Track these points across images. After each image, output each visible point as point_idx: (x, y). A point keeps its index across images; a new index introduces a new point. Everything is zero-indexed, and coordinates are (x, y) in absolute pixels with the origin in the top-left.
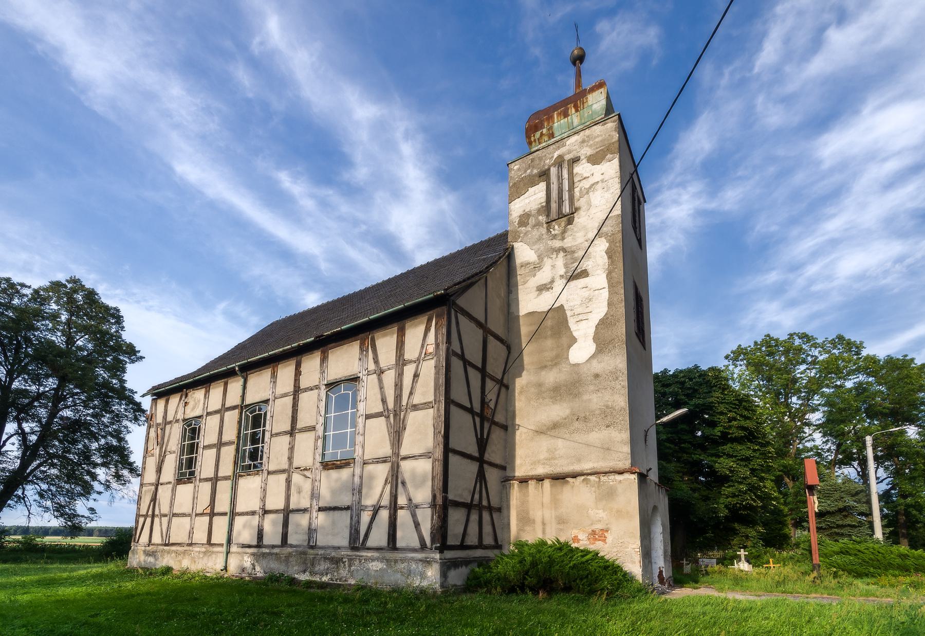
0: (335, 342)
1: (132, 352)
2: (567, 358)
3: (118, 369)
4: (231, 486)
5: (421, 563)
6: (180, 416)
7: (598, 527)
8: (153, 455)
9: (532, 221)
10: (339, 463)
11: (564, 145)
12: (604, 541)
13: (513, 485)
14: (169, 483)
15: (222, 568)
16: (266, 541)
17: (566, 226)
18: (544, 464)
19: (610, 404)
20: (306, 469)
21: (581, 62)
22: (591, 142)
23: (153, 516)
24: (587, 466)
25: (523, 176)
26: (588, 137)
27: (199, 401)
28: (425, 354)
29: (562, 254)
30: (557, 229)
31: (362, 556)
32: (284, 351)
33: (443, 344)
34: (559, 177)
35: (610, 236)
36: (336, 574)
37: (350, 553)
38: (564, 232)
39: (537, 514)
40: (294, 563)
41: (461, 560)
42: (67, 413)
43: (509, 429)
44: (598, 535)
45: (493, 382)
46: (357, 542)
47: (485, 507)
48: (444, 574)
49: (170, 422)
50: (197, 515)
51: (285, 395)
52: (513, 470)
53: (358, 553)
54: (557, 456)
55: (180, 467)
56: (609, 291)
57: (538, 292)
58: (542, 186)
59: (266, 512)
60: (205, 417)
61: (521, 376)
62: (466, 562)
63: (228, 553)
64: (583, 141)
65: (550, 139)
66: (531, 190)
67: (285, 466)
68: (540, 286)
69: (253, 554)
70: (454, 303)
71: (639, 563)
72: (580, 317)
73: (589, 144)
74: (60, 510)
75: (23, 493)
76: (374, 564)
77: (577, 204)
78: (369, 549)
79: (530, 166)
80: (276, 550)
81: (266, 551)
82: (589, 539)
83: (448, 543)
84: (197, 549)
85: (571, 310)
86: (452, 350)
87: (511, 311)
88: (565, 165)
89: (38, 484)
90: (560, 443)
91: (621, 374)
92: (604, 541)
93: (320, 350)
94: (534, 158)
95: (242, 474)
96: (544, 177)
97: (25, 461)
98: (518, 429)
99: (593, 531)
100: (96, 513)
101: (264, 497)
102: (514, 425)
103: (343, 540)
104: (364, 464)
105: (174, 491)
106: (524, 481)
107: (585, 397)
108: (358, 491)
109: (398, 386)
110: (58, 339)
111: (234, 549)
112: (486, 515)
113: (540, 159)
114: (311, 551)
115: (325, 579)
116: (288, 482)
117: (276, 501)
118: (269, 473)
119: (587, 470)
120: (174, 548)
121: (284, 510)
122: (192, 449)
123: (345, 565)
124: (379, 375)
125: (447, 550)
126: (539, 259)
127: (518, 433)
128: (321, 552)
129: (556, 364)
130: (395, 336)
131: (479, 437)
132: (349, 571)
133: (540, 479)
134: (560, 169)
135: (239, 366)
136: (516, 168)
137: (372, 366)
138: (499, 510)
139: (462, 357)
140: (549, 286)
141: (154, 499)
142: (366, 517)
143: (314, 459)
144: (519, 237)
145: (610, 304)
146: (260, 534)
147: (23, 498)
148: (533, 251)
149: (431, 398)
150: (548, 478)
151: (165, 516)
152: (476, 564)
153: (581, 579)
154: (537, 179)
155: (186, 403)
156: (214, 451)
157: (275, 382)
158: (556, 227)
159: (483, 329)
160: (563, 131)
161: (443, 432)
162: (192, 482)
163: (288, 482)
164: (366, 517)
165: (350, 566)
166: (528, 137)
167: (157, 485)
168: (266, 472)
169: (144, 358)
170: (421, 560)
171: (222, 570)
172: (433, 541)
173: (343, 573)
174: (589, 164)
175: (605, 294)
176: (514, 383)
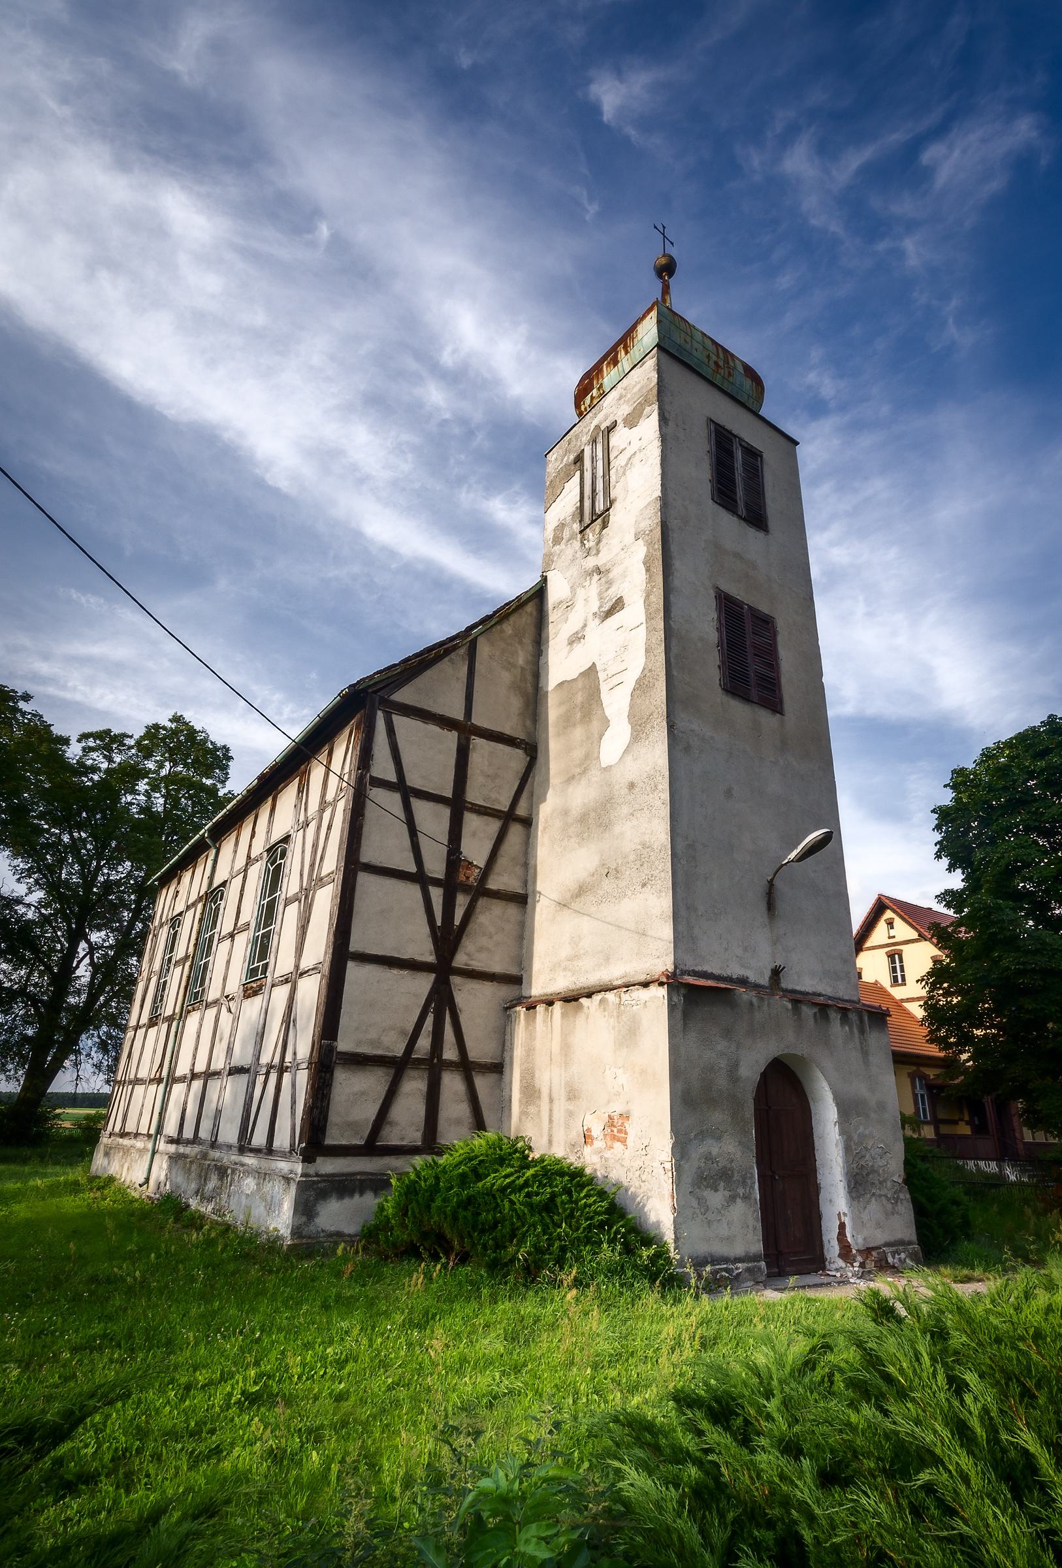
7: (617, 1107)
9: (566, 534)
12: (623, 1141)
17: (600, 533)
18: (565, 969)
19: (647, 838)
21: (671, 275)
24: (614, 973)
29: (596, 577)
34: (593, 458)
38: (599, 542)
41: (363, 1178)
43: (529, 900)
47: (450, 1065)
48: (305, 1208)
54: (582, 952)
61: (544, 800)
63: (154, 1153)
71: (670, 1200)
72: (615, 681)
82: (605, 1135)
83: (329, 1141)
88: (600, 439)
91: (661, 778)
92: (623, 1141)
102: (534, 892)
107: (617, 829)
109: (315, 846)
112: (452, 1084)
125: (324, 1155)
131: (439, 923)
138: (498, 1068)
139: (401, 787)
140: (580, 635)
150: (543, 1002)
154: (573, 467)
159: (456, 729)
166: (577, 406)
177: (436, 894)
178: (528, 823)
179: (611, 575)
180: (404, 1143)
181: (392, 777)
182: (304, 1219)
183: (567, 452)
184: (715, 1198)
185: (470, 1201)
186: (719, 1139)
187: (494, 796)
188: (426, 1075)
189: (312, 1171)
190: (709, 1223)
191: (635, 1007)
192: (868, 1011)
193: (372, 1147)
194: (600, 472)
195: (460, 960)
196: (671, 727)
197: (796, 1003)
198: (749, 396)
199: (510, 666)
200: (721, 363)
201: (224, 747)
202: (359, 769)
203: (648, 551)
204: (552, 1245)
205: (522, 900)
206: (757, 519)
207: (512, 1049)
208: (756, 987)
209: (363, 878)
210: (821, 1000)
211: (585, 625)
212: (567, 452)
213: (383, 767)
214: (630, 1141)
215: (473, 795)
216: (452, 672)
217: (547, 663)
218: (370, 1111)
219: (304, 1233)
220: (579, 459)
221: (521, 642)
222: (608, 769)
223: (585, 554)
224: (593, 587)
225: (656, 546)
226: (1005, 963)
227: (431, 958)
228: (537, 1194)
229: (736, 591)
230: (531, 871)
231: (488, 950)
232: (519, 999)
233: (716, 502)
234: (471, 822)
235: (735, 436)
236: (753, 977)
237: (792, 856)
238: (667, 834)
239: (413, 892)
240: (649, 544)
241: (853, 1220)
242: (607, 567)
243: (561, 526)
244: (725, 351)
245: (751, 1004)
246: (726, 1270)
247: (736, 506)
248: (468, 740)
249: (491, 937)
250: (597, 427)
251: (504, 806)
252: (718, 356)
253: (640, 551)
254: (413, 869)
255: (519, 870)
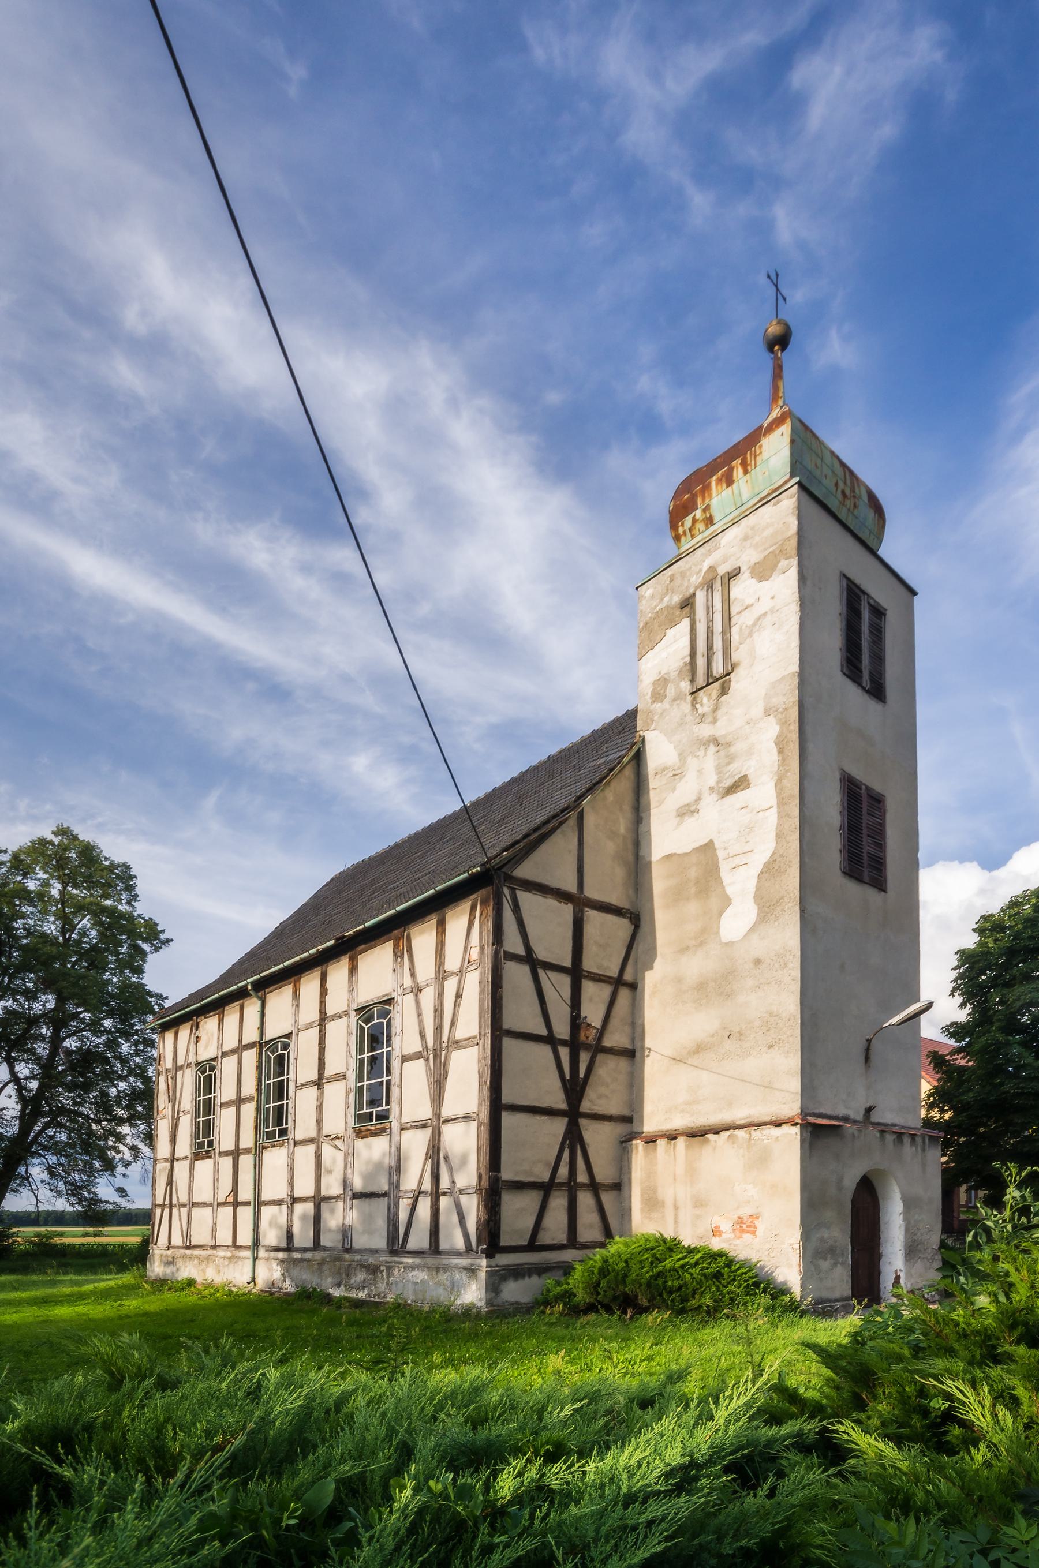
0: (365, 943)
1: (153, 933)
2: (718, 933)
3: (135, 962)
4: (252, 1163)
5: (465, 1272)
6: (192, 1059)
7: (745, 1211)
8: (164, 1117)
9: (671, 691)
10: (373, 1128)
11: (717, 547)
12: (753, 1233)
13: (637, 1148)
14: (186, 1158)
15: (249, 1280)
16: (297, 1242)
18: (683, 1111)
20: (337, 1138)
22: (757, 539)
23: (171, 1206)
24: (739, 1115)
25: (658, 609)
26: (752, 528)
27: (212, 1035)
28: (469, 962)
29: (712, 749)
30: (706, 700)
31: (401, 1263)
32: (301, 959)
33: (488, 946)
34: (708, 608)
35: (782, 713)
36: (373, 1288)
37: (389, 1259)
38: (716, 709)
39: (667, 1193)
40: (327, 1272)
42: (71, 1044)
43: (637, 1054)
44: (745, 1225)
45: (603, 985)
46: (396, 1245)
47: (583, 1186)
49: (181, 1067)
50: (219, 1204)
51: (309, 1026)
52: (641, 1122)
53: (397, 1259)
55: (197, 1136)
56: (778, 813)
57: (678, 818)
58: (686, 622)
59: (294, 1200)
60: (220, 1059)
61: (651, 968)
62: (541, 1270)
64: (746, 538)
65: (707, 528)
66: (670, 633)
67: (313, 1134)
68: (681, 807)
69: (282, 1261)
70: (509, 878)
71: (798, 1267)
72: (738, 861)
73: (755, 542)
74: (75, 1191)
75: (26, 1172)
76: (414, 1273)
77: (735, 658)
78: (409, 1253)
79: (667, 590)
80: (308, 1255)
81: (297, 1255)
82: (734, 1230)
83: (503, 1243)
84: (221, 1253)
85: (725, 849)
86: (505, 952)
87: (641, 854)
88: (717, 585)
89: (44, 1157)
90: (705, 1076)
91: (791, 957)
92: (753, 1233)
93: (348, 955)
94: (673, 575)
95: (266, 1144)
96: (687, 610)
97: (26, 1120)
98: (648, 1056)
99: (739, 1218)
100: (127, 1195)
101: (292, 1178)
102: (643, 1048)
103: (380, 1242)
104: (402, 1129)
105: (192, 1168)
106: (651, 1140)
108: (397, 1169)
109: (439, 1012)
110: (51, 927)
111: (262, 1253)
112: (585, 1199)
113: (683, 575)
114: (347, 1256)
115: (362, 1295)
116: (318, 1156)
117: (305, 1187)
118: (296, 1143)
119: (740, 1120)
120: (196, 1252)
121: (314, 1197)
122: (208, 1107)
123: (383, 1276)
124: (416, 995)
125: (500, 1253)
126: (680, 760)
127: (648, 1062)
128: (357, 1257)
129: (701, 944)
130: (434, 932)
131: (568, 1077)
132: (388, 1284)
133: (672, 1137)
134: (710, 594)
135: (252, 983)
136: (649, 593)
137: (408, 982)
138: (619, 1186)
139: (529, 959)
140: (693, 808)
141: (170, 1182)
142: (405, 1203)
143: (346, 1122)
144: (653, 721)
145: (779, 836)
146: (290, 1236)
147: (27, 1179)
148: (672, 745)
149: (474, 1031)
150: (662, 1136)
151: (184, 1206)
152: (561, 1272)
153: (670, 1293)
154: (678, 612)
155: (197, 1037)
156: (233, 1109)
157: (297, 1006)
158: (705, 700)
160: (728, 511)
161: (488, 1083)
162: (210, 1157)
163: (318, 1156)
164: (405, 1203)
165: (388, 1277)
166: (674, 525)
167: (172, 1160)
168: (291, 1142)
169: (172, 940)
170: (465, 1268)
171: (248, 1283)
172: (479, 1243)
173: (382, 1286)
174: (754, 581)
175: (772, 816)
176: (643, 978)
177: (564, 1052)
178: (633, 986)
179: (732, 749)
180: (555, 1242)
181: (521, 951)
182: (493, 1294)
183: (668, 590)
184: (825, 1265)
185: (659, 1275)
186: (828, 1228)
187: (605, 963)
188: (566, 1194)
189: (493, 1264)
190: (821, 1279)
191: (765, 1141)
192: (929, 1136)
193: (532, 1246)
194: (718, 627)
195: (586, 1106)
196: (803, 911)
197: (882, 1132)
198: (871, 532)
199: (613, 835)
200: (848, 492)
201: (124, 864)
202: (493, 944)
203: (781, 731)
204: (723, 1297)
205: (632, 1054)
206: (877, 691)
207: (630, 1173)
208: (855, 1122)
209: (507, 1043)
210: (896, 1129)
211: (699, 799)
212: (668, 590)
213: (513, 943)
214: (760, 1232)
215: (589, 964)
216: (563, 844)
217: (649, 832)
218: (530, 1222)
219: (495, 1304)
220: (688, 604)
221: (621, 809)
222: (730, 944)
223: (697, 720)
224: (709, 760)
225: (792, 728)
226: (1006, 1088)
227: (563, 1106)
228: (708, 1268)
229: (857, 773)
230: (638, 1030)
231: (607, 1097)
232: (631, 1134)
233: (844, 674)
234: (589, 988)
235: (864, 593)
236: (852, 1115)
237: (894, 1020)
238: (797, 1005)
239: (545, 1051)
240: (783, 723)
241: (906, 1274)
242: (728, 740)
243: (662, 682)
244: (852, 473)
245: (853, 1135)
246: (830, 1306)
247: (861, 677)
248: (582, 912)
249: (608, 1086)
250: (712, 569)
251: (614, 973)
252: (845, 483)
253: (771, 729)
254: (544, 1032)
255: (627, 1029)
